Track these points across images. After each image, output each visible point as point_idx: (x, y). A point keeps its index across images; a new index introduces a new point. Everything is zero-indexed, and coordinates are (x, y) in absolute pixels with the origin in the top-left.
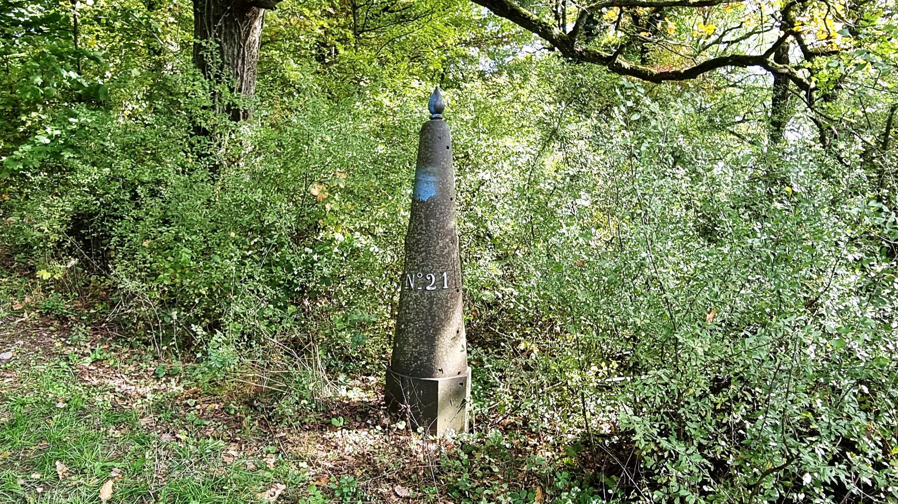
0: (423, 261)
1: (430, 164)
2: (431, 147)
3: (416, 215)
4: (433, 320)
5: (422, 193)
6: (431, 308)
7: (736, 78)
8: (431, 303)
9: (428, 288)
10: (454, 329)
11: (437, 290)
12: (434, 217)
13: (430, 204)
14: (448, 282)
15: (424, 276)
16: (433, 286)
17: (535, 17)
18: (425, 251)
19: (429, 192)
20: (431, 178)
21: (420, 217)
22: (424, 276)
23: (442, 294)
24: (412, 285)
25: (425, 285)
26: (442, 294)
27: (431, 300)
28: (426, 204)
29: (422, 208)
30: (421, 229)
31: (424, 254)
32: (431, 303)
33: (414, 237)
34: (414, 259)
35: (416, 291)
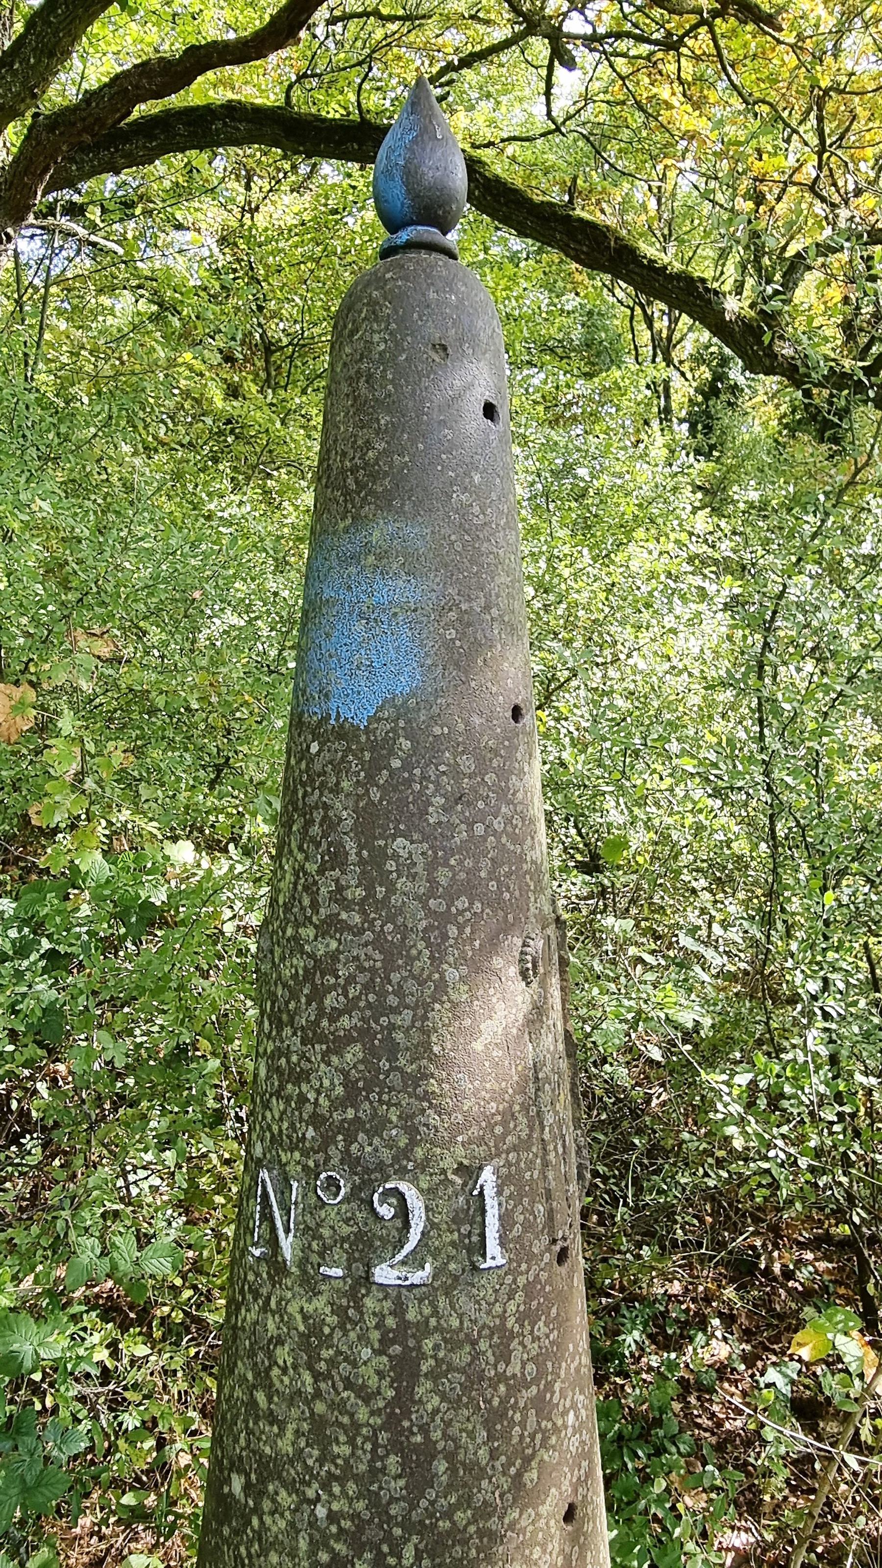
0: (351, 1097)
1: (385, 502)
2: (390, 405)
3: (306, 812)
4: (418, 1478)
5: (338, 682)
6: (404, 1400)
7: (578, 277)
8: (405, 1370)
9: (385, 1274)
10: (552, 1506)
11: (446, 1284)
12: (412, 820)
13: (387, 746)
14: (506, 1220)
15: (361, 1196)
16: (415, 1261)
17: (677, 266)
18: (364, 1034)
19: (375, 676)
20: (398, 589)
21: (330, 824)
22: (361, 1196)
23: (466, 1310)
24: (287, 1245)
25: (365, 1248)
26: (466, 1310)
27: (402, 1344)
28: (364, 747)
29: (340, 767)
30: (338, 894)
31: (353, 1054)
32: (405, 1370)
33: (296, 944)
34: (302, 1076)
35: (310, 1283)
